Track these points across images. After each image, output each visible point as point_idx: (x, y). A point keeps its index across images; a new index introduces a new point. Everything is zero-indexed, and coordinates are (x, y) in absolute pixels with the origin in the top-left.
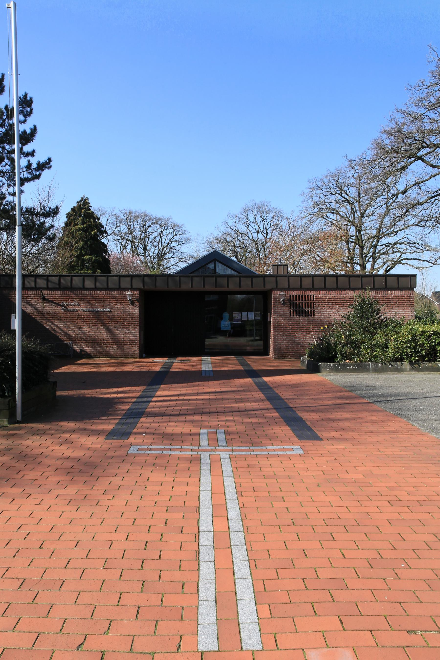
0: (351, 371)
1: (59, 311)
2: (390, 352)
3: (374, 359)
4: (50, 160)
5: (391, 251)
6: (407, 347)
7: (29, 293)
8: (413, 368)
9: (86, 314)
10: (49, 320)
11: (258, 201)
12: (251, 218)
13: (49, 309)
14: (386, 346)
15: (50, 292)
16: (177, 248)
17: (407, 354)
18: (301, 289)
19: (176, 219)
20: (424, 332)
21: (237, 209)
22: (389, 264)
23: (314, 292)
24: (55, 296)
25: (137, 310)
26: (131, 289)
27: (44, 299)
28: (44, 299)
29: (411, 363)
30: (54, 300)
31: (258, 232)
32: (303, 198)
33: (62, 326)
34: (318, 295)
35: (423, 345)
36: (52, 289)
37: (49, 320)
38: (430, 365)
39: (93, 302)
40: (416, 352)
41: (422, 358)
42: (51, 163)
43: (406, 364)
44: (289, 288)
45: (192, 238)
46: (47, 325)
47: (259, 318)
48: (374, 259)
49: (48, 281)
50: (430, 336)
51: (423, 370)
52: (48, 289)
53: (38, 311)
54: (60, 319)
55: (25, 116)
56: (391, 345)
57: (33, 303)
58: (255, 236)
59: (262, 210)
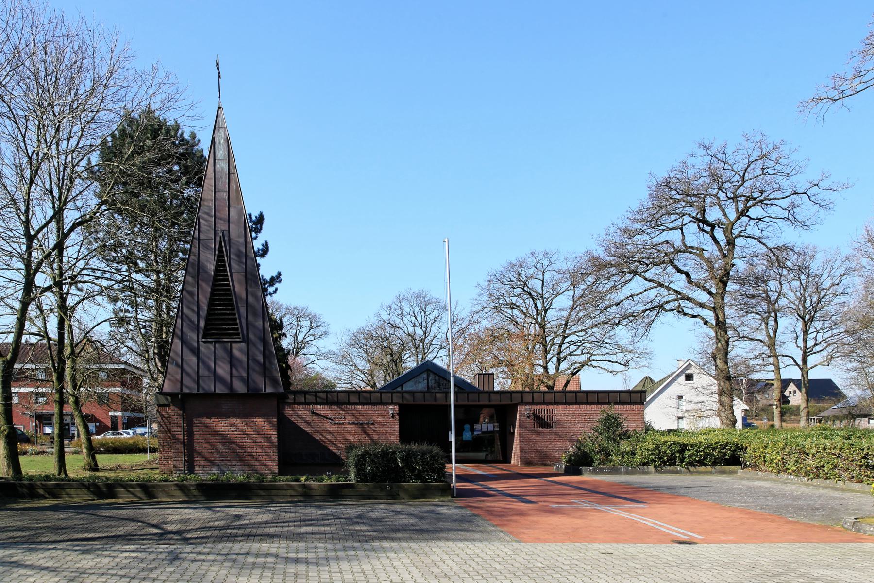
0: (607, 473)
1: (327, 424)
2: (638, 458)
3: (626, 464)
4: (279, 274)
5: (579, 352)
6: (652, 454)
7: (299, 407)
8: (657, 471)
9: (351, 426)
10: (318, 432)
11: (416, 289)
12: (407, 309)
13: (317, 422)
14: (633, 453)
15: (318, 406)
16: (314, 342)
17: (652, 460)
18: (544, 403)
19: (313, 309)
20: (665, 442)
21: (390, 299)
22: (577, 365)
23: (554, 407)
24: (323, 410)
25: (397, 422)
26: (392, 403)
27: (313, 413)
28: (313, 413)
29: (655, 467)
30: (322, 414)
31: (414, 326)
32: (478, 290)
33: (329, 437)
34: (559, 409)
35: (665, 452)
36: (320, 404)
37: (318, 432)
38: (670, 468)
39: (357, 415)
40: (659, 458)
41: (664, 462)
42: (282, 277)
43: (651, 468)
44: (533, 403)
45: (330, 331)
46: (317, 436)
47: (497, 429)
48: (559, 360)
49: (316, 396)
50: (671, 445)
51: (664, 473)
52: (317, 403)
53: (308, 424)
54: (328, 432)
55: (256, 233)
56: (639, 452)
57: (303, 416)
58: (411, 329)
59: (423, 301)
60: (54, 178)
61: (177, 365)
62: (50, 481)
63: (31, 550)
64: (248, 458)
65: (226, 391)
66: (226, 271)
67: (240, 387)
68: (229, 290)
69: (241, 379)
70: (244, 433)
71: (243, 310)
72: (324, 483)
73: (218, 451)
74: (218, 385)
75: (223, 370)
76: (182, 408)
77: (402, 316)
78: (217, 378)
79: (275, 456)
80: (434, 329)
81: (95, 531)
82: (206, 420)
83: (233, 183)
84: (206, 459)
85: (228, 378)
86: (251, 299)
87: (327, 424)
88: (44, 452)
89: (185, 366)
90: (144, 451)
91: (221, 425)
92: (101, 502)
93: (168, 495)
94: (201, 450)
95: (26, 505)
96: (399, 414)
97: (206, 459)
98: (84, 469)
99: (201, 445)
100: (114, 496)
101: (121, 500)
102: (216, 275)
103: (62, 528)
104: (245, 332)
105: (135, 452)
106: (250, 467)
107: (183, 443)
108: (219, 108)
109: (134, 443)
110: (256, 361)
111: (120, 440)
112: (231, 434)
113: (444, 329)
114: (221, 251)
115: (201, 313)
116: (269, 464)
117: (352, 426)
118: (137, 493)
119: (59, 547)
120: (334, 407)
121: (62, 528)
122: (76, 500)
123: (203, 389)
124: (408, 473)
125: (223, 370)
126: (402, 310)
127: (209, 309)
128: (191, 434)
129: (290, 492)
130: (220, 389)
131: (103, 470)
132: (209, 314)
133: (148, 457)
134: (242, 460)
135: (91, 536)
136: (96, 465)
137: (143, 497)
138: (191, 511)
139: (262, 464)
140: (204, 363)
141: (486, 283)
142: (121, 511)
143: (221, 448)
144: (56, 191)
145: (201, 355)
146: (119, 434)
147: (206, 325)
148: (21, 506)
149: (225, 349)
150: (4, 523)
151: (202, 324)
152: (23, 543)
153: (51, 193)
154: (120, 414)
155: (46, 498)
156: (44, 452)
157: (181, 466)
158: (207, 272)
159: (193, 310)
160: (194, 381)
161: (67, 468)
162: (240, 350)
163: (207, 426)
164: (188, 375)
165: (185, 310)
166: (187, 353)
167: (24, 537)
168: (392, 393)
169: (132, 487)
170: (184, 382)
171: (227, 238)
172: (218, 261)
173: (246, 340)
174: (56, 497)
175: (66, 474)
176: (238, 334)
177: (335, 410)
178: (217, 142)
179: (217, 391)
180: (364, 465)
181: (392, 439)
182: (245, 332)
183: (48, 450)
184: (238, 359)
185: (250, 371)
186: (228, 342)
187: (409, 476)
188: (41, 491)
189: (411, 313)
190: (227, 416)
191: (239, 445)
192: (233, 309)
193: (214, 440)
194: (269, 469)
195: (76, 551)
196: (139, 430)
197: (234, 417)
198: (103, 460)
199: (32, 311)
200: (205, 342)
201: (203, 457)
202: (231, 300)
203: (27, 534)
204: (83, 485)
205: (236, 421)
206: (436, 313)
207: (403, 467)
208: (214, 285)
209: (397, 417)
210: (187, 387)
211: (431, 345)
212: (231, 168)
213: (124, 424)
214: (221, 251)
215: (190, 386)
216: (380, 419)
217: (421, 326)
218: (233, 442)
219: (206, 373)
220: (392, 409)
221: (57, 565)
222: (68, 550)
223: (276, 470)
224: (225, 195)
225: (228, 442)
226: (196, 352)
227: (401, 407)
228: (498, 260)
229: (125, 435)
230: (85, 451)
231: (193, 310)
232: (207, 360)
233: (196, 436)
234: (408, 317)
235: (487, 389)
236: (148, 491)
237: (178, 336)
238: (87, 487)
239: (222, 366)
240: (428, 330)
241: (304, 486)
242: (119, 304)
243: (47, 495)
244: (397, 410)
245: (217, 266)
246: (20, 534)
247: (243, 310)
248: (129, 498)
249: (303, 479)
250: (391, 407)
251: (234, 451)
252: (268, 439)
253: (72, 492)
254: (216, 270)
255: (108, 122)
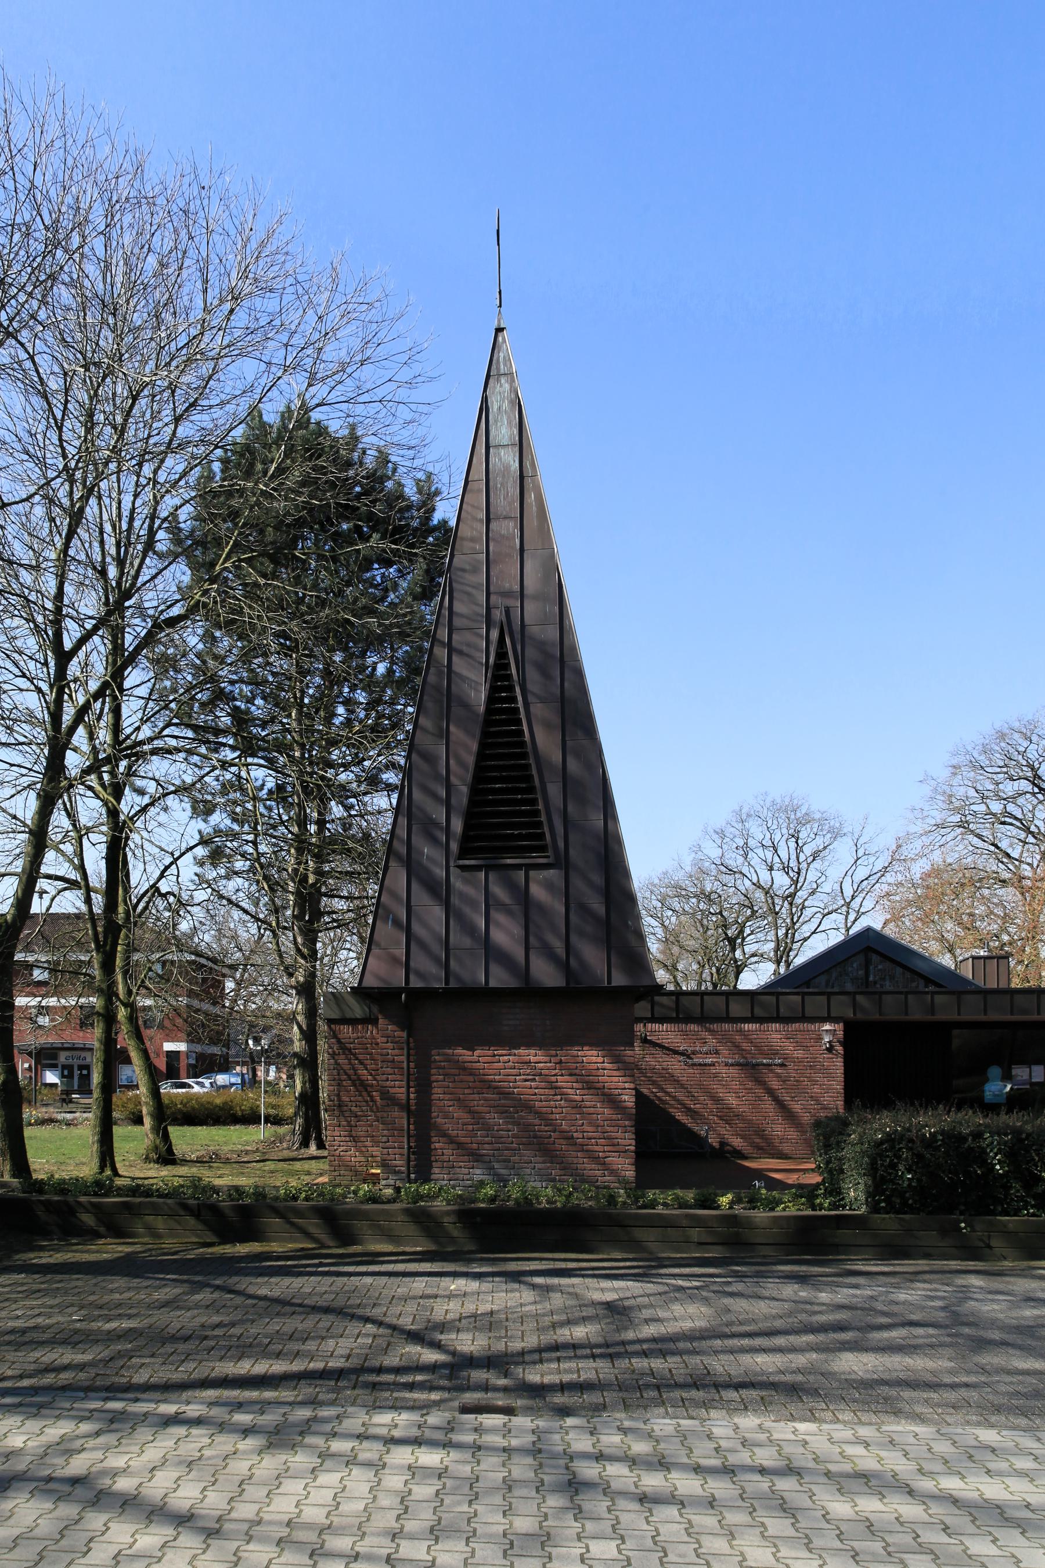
1: (675, 1065)
12: (757, 832)
15: (656, 1026)
21: (721, 816)
25: (839, 1064)
30: (665, 1043)
32: (927, 790)
33: (681, 1095)
36: (662, 1020)
52: (653, 1020)
58: (765, 877)
60: (110, 542)
61: (397, 923)
62: (106, 1195)
63: (115, 1420)
64: (561, 1145)
65: (512, 983)
66: (514, 700)
67: (545, 974)
68: (523, 744)
69: (550, 954)
70: (552, 1086)
71: (554, 790)
72: (779, 1211)
73: (487, 1128)
74: (496, 970)
75: (506, 934)
76: (406, 1024)
77: (746, 851)
78: (491, 952)
79: (628, 1140)
80: (812, 875)
81: (265, 1353)
82: (463, 1054)
83: (531, 498)
84: (460, 1145)
85: (519, 953)
86: (573, 765)
87: (675, 1065)
88: (51, 1121)
89: (416, 927)
90: (251, 1118)
91: (484, 1059)
92: (228, 1249)
93: (390, 1237)
94: (448, 1126)
95: (59, 1257)
96: (845, 1043)
97: (460, 1145)
98: (147, 1159)
99: (449, 1114)
100: (252, 1234)
101: (275, 1247)
102: (489, 710)
103: (174, 1338)
104: (561, 844)
105: (225, 1123)
106: (567, 1168)
107: (406, 1108)
108: (499, 330)
109: (225, 1103)
110: (584, 908)
111: (190, 1097)
112: (524, 1087)
113: (835, 873)
114: (501, 654)
115: (453, 801)
116: (616, 1162)
117: (733, 1071)
118: (312, 1230)
119: (193, 1410)
120: (693, 1027)
121: (174, 1338)
122: (169, 1243)
123: (459, 979)
124: (1016, 1188)
125: (506, 934)
126: (746, 837)
127: (474, 791)
128: (423, 1085)
129: (695, 1234)
130: (500, 978)
131: (184, 1162)
132: (472, 803)
133: (261, 1132)
134: (547, 1152)
135: (261, 1368)
136: (170, 1150)
137: (324, 1238)
138: (474, 1285)
139: (595, 1159)
140: (461, 918)
141: (946, 773)
142: (297, 1282)
143: (496, 1120)
144: (112, 572)
145: (455, 900)
146: (184, 1085)
147: (467, 827)
148: (46, 1258)
149: (511, 886)
150: (18, 1315)
151: (457, 825)
152: (88, 1390)
153: (103, 573)
154: (182, 1047)
155: (100, 1236)
156: (51, 1121)
157: (400, 1163)
158: (466, 705)
159: (435, 796)
160: (436, 960)
161: (117, 1159)
162: (549, 886)
163: (463, 1068)
164: (423, 946)
165: (417, 794)
166: (421, 897)
167: (82, 1367)
168: (829, 995)
169: (299, 1213)
170: (412, 964)
171: (517, 626)
172: (495, 678)
173: (563, 863)
174: (119, 1233)
175: (115, 1173)
176: (543, 849)
177: (696, 1033)
178: (494, 407)
179: (493, 984)
180: (893, 1166)
181: (826, 1100)
182: (561, 844)
183: (60, 1117)
184: (541, 908)
185: (574, 939)
186: (518, 867)
187: (1021, 1199)
188: (88, 1219)
189: (767, 842)
190: (512, 1043)
191: (539, 1114)
192: (531, 790)
193: (478, 1102)
194: (613, 1172)
195: (247, 1431)
196: (222, 1079)
197: (529, 1046)
198: (187, 1139)
199: (59, 820)
200: (463, 868)
201: (452, 1141)
202: (527, 767)
203: (87, 1357)
204: (185, 1207)
205: (534, 1055)
206: (819, 843)
207: (1006, 1174)
208: (485, 734)
209: (840, 1049)
210: (420, 975)
211: (804, 907)
212: (527, 464)
213: (189, 1065)
214: (501, 654)
215: (429, 974)
216: (799, 1054)
217: (786, 869)
218: (527, 1107)
219: (467, 942)
220: (829, 1032)
221: (215, 1501)
222: (222, 1427)
223: (630, 1173)
224: (510, 528)
225: (514, 1106)
226: (441, 892)
227: (851, 1028)
228: (973, 726)
229: (197, 1089)
230: (148, 1121)
231: (435, 796)
232: (467, 910)
233: (437, 1093)
234: (760, 851)
235: (1003, 985)
236: (336, 1227)
237: (399, 857)
238: (196, 1212)
239: (498, 929)
240: (801, 879)
241: (732, 1220)
242: (216, 818)
243: (102, 1230)
244: (840, 1034)
245: (493, 690)
246: (68, 1356)
247: (554, 790)
248: (292, 1240)
249: (725, 1200)
250: (827, 1027)
251: (526, 1128)
252: (612, 1101)
253: (160, 1223)
254: (491, 700)
255: (221, 417)
